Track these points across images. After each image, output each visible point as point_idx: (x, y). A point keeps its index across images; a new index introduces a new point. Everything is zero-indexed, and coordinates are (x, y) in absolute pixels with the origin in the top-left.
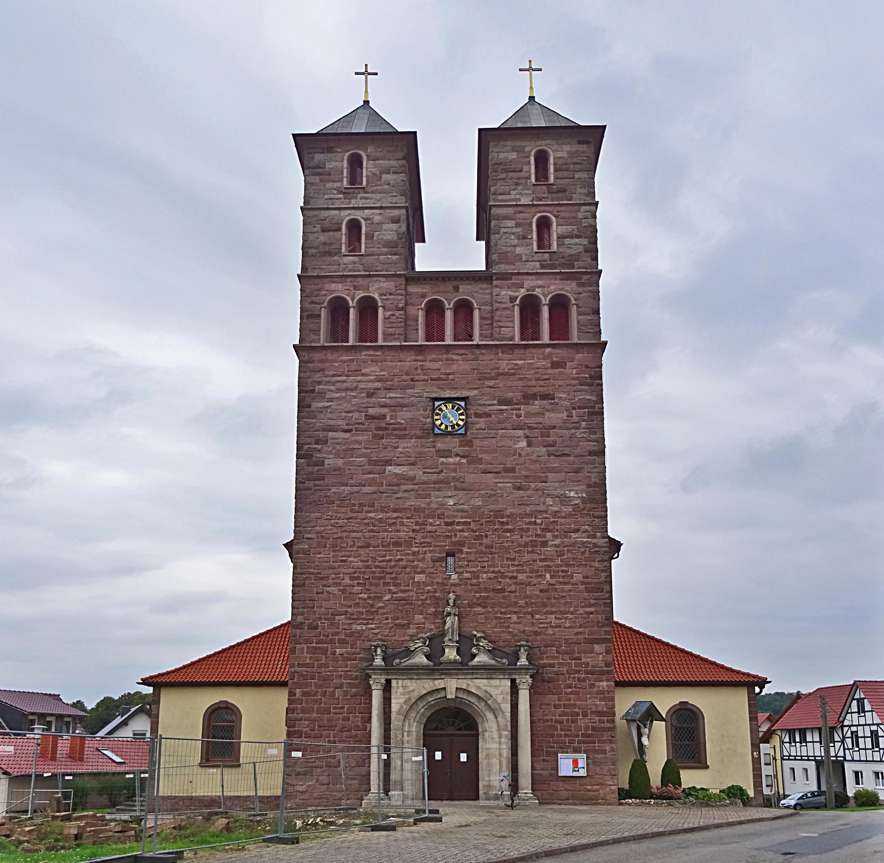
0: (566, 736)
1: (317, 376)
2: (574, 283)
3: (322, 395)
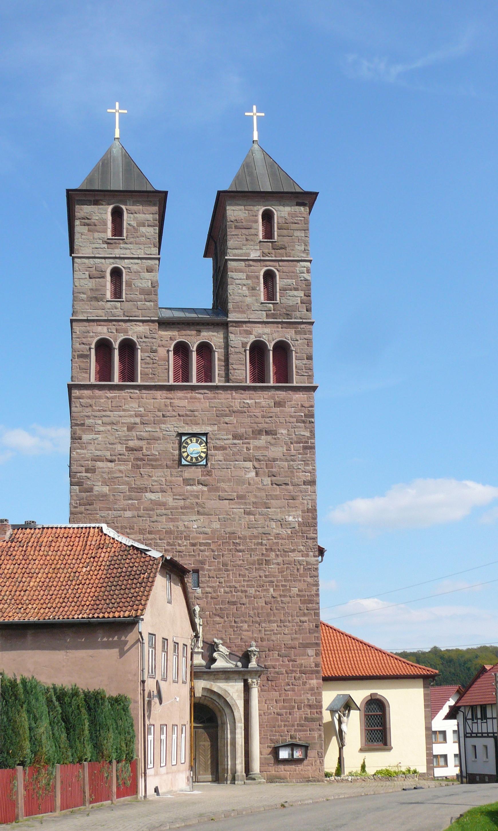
0: (285, 726)
1: (88, 412)
2: (293, 331)
3: (90, 429)
